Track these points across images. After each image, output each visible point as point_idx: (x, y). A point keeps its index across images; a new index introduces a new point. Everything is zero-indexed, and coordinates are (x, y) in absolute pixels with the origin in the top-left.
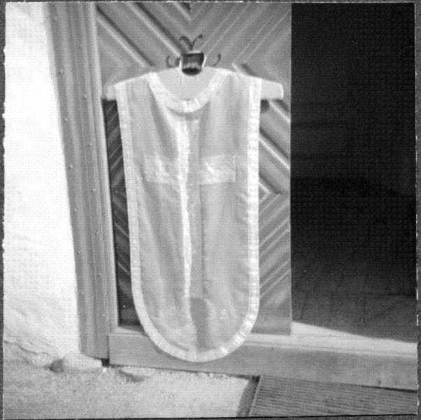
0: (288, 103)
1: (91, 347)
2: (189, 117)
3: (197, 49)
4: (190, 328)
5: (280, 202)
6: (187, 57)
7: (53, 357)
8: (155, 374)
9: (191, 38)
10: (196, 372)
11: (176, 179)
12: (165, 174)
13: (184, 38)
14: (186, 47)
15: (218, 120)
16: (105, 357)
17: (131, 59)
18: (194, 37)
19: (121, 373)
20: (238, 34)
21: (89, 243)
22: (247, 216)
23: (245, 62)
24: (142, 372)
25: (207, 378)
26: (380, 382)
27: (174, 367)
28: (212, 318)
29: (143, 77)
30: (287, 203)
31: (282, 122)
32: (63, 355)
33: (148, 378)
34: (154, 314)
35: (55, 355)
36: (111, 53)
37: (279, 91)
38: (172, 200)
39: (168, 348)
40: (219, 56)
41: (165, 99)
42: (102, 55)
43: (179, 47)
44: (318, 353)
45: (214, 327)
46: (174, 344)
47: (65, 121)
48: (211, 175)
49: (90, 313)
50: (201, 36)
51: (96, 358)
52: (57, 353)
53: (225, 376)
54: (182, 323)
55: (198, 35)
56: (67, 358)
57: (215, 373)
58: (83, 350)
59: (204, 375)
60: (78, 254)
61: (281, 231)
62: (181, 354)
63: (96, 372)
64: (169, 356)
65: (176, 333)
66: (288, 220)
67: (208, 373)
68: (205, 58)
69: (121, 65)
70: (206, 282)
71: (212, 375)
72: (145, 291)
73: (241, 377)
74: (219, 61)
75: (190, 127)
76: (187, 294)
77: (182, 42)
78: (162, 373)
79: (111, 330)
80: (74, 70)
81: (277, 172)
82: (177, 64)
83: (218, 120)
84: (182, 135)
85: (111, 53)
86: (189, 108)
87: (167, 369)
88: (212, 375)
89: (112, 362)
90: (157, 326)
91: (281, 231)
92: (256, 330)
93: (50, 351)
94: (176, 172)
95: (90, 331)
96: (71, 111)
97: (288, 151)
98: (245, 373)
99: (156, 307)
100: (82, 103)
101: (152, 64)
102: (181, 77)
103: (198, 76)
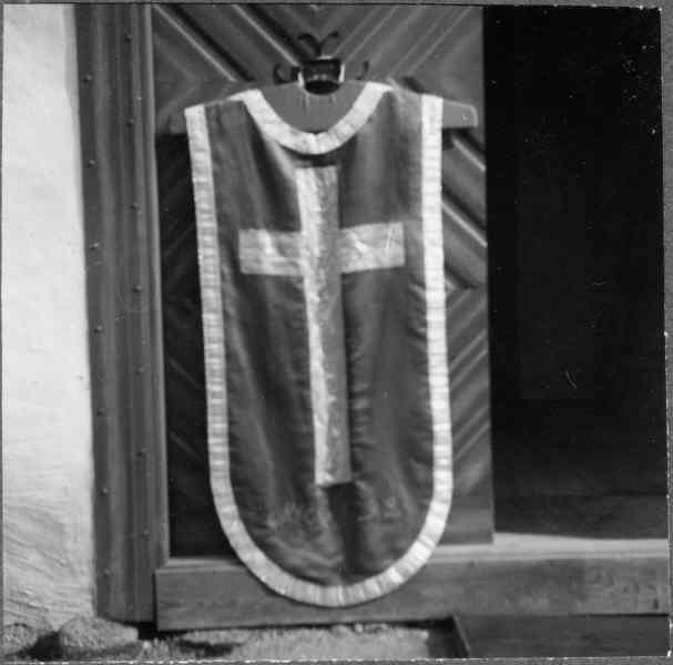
0: (481, 138)
1: (118, 601)
2: (317, 161)
3: (328, 54)
4: (329, 539)
5: (472, 302)
6: (309, 65)
7: (39, 631)
8: (250, 638)
9: (319, 36)
10: (327, 626)
11: (296, 265)
12: (280, 259)
13: (308, 37)
14: (310, 51)
15: (371, 164)
16: (148, 617)
17: (210, 69)
18: (324, 37)
19: (187, 647)
20: (403, 26)
21: (124, 401)
22: (425, 324)
23: (409, 74)
24: (223, 637)
25: (350, 634)
26: (656, 605)
27: (288, 620)
28: (369, 517)
29: (236, 98)
30: (482, 305)
31: (469, 167)
32: (62, 622)
33: (239, 645)
34: (254, 526)
35: (43, 627)
36: (175, 60)
37: (471, 118)
38: (293, 306)
39: (283, 583)
40: (366, 65)
41: (276, 131)
42: (157, 63)
43: (296, 51)
44: (552, 563)
45: (375, 535)
46: (297, 573)
47: (90, 165)
48: (360, 255)
49: (118, 539)
50: (335, 35)
51: (128, 623)
52: (44, 621)
53: (384, 626)
54: (311, 534)
55: (330, 32)
56: (68, 630)
57: (364, 623)
58: (102, 608)
59: (343, 629)
60: (99, 414)
61: (474, 353)
62: (312, 593)
63: (129, 650)
64: (292, 601)
65: (300, 555)
66: (482, 336)
67: (351, 625)
68: (343, 69)
69: (191, 77)
70: (356, 449)
71: (359, 628)
72: (238, 481)
73: (411, 625)
74: (365, 73)
75: (321, 177)
76: (322, 477)
77: (303, 43)
78: (266, 635)
79: (160, 563)
80: (112, 80)
81: (466, 251)
82: (295, 78)
83: (371, 164)
84: (308, 190)
85: (175, 60)
86: (319, 144)
87: (272, 627)
88: (359, 628)
89: (162, 625)
90: (262, 544)
91: (474, 353)
92: (446, 539)
93: (32, 621)
94: (297, 254)
95: (117, 568)
96: (101, 106)
97: (483, 216)
98: (421, 615)
99: (263, 512)
100: (123, 129)
101: (247, 78)
102: (304, 96)
103: (334, 96)
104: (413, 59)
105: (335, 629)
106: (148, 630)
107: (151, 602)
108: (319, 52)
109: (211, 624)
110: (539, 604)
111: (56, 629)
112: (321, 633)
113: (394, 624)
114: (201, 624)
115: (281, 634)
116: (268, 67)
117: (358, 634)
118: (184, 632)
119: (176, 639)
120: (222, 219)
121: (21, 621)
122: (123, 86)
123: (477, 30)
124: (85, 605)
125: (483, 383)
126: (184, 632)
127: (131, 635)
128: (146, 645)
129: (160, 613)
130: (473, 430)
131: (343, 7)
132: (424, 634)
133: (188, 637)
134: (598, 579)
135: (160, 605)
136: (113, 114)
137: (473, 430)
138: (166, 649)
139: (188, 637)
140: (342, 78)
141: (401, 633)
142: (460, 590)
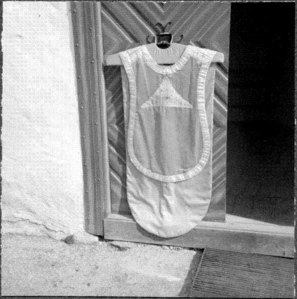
1: (92, 227)
9: (164, 24)
13: (159, 24)
17: (123, 38)
18: (165, 24)
26: (284, 254)
30: (225, 134)
44: (243, 233)
58: (87, 229)
59: (166, 247)
60: (85, 165)
61: (221, 152)
63: (95, 243)
66: (225, 145)
67: (169, 246)
73: (191, 249)
77: (157, 27)
89: (105, 238)
91: (221, 152)
95: (91, 217)
97: (226, 99)
98: (194, 246)
104: (200, 35)
105: (163, 247)
106: (101, 238)
107: (278, 259)
108: (163, 31)
109: (121, 239)
110: (238, 247)
111: (72, 234)
112: (159, 247)
113: (184, 248)
114: (118, 239)
115: (145, 246)
116: (144, 37)
117: (171, 249)
118: (112, 240)
119: (110, 242)
120: (104, 48)
121: (62, 230)
122: (89, 47)
123: (230, 7)
124: (81, 226)
125: (224, 163)
126: (112, 240)
127: (97, 239)
128: (101, 243)
129: (105, 233)
130: (220, 180)
131: (183, 183)
132: (194, 253)
133: (114, 243)
134: (261, 242)
135: (105, 231)
136: (87, 58)
137: (220, 180)
138: (106, 245)
139: (114, 243)
140: (171, 43)
141: (186, 251)
142: (208, 239)
